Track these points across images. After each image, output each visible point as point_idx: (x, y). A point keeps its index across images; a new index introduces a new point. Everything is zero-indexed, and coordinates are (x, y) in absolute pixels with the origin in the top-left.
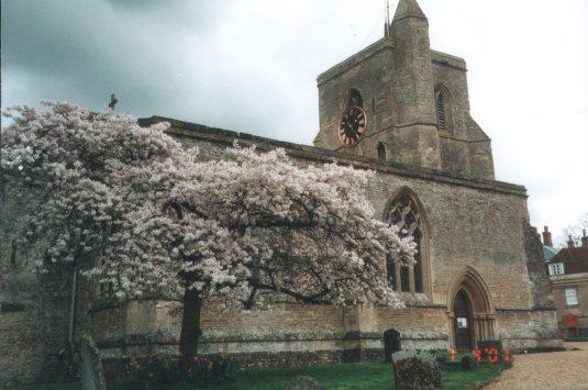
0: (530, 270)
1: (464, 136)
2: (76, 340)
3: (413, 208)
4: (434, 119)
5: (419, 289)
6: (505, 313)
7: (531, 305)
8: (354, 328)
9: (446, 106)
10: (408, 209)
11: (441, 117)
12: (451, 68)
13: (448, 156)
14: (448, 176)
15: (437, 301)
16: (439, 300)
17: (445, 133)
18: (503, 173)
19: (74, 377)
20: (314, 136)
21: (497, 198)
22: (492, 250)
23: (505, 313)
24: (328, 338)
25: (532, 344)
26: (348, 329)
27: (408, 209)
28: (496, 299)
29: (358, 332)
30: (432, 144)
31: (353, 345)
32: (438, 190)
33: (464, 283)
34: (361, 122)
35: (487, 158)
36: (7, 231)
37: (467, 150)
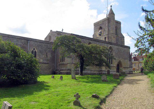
0: (129, 61)
1: (120, 36)
2: (57, 69)
3: (112, 50)
4: (115, 33)
5: (112, 64)
6: (125, 68)
7: (129, 67)
8: (101, 69)
9: (117, 30)
10: (111, 50)
11: (116, 33)
12: (119, 23)
13: (117, 40)
14: (116, 44)
15: (115, 66)
16: (114, 66)
17: (117, 36)
18: (126, 44)
19: (1, 53)
20: (92, 33)
21: (125, 49)
22: (124, 57)
23: (125, 68)
24: (97, 71)
25: (128, 73)
26: (100, 70)
27: (111, 50)
28: (123, 66)
29: (102, 70)
30: (114, 37)
31: (101, 72)
32: (116, 47)
33: (119, 63)
34: (102, 33)
35: (123, 40)
36: (46, 51)
37: (120, 39)
